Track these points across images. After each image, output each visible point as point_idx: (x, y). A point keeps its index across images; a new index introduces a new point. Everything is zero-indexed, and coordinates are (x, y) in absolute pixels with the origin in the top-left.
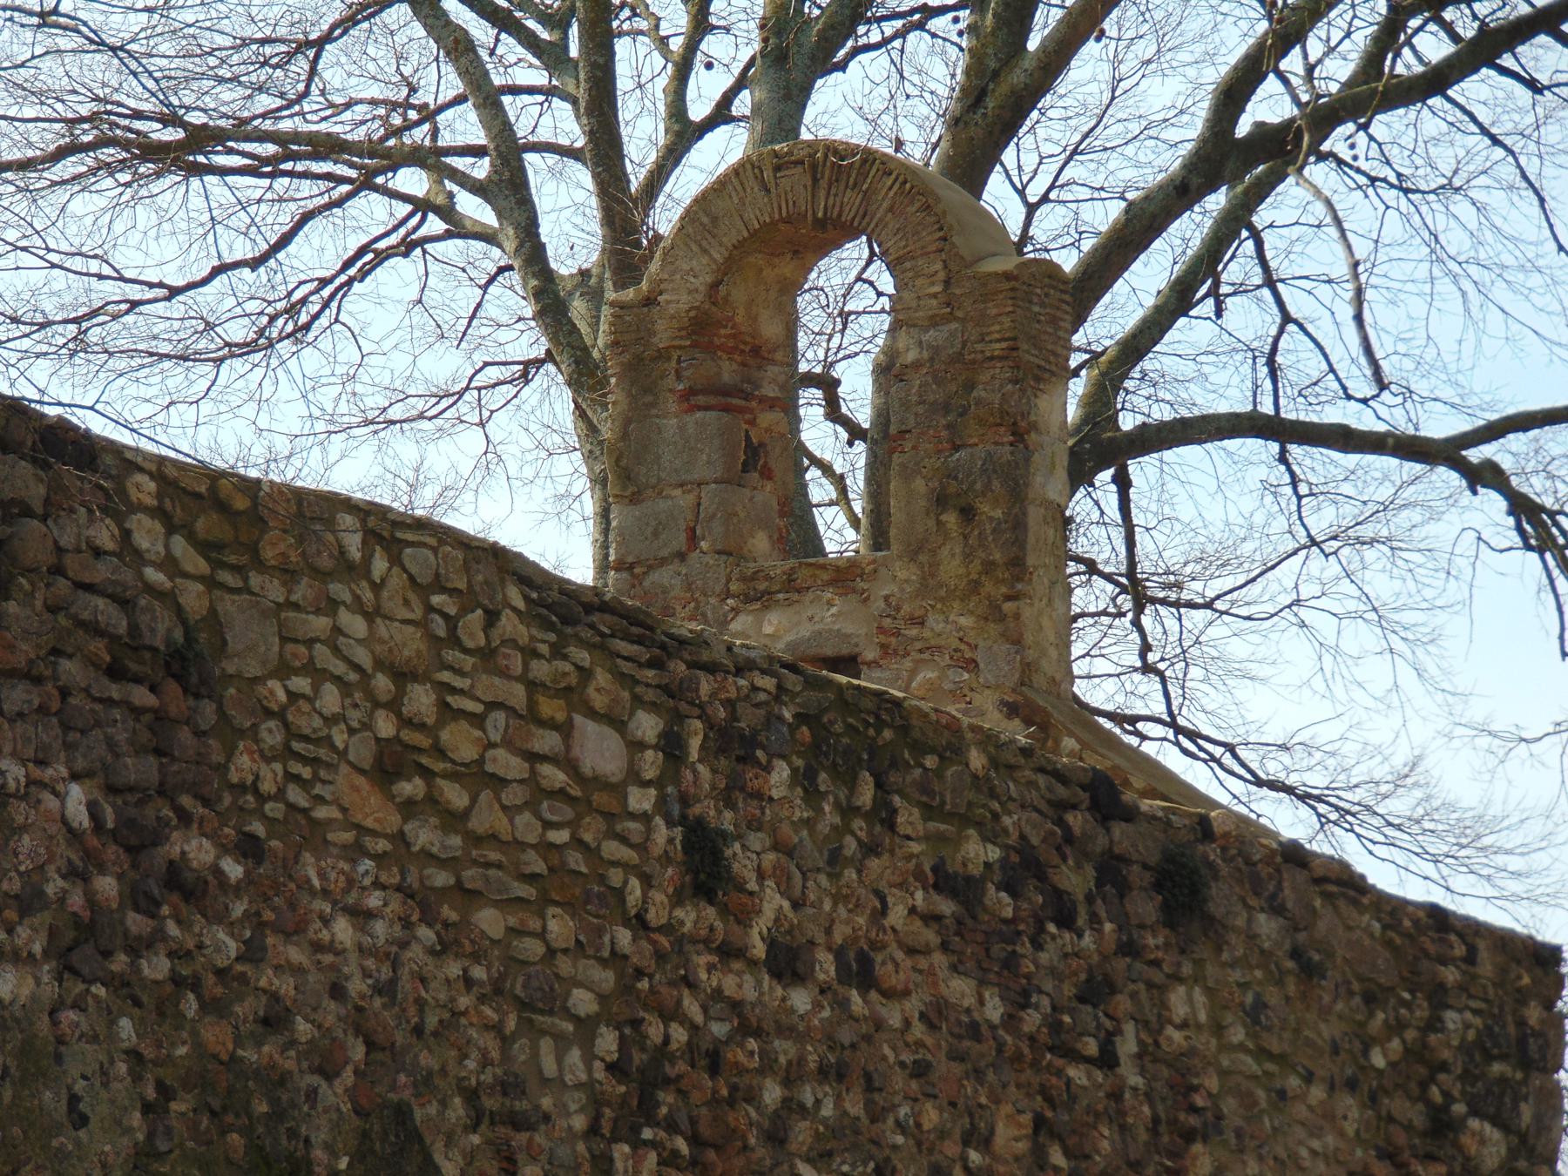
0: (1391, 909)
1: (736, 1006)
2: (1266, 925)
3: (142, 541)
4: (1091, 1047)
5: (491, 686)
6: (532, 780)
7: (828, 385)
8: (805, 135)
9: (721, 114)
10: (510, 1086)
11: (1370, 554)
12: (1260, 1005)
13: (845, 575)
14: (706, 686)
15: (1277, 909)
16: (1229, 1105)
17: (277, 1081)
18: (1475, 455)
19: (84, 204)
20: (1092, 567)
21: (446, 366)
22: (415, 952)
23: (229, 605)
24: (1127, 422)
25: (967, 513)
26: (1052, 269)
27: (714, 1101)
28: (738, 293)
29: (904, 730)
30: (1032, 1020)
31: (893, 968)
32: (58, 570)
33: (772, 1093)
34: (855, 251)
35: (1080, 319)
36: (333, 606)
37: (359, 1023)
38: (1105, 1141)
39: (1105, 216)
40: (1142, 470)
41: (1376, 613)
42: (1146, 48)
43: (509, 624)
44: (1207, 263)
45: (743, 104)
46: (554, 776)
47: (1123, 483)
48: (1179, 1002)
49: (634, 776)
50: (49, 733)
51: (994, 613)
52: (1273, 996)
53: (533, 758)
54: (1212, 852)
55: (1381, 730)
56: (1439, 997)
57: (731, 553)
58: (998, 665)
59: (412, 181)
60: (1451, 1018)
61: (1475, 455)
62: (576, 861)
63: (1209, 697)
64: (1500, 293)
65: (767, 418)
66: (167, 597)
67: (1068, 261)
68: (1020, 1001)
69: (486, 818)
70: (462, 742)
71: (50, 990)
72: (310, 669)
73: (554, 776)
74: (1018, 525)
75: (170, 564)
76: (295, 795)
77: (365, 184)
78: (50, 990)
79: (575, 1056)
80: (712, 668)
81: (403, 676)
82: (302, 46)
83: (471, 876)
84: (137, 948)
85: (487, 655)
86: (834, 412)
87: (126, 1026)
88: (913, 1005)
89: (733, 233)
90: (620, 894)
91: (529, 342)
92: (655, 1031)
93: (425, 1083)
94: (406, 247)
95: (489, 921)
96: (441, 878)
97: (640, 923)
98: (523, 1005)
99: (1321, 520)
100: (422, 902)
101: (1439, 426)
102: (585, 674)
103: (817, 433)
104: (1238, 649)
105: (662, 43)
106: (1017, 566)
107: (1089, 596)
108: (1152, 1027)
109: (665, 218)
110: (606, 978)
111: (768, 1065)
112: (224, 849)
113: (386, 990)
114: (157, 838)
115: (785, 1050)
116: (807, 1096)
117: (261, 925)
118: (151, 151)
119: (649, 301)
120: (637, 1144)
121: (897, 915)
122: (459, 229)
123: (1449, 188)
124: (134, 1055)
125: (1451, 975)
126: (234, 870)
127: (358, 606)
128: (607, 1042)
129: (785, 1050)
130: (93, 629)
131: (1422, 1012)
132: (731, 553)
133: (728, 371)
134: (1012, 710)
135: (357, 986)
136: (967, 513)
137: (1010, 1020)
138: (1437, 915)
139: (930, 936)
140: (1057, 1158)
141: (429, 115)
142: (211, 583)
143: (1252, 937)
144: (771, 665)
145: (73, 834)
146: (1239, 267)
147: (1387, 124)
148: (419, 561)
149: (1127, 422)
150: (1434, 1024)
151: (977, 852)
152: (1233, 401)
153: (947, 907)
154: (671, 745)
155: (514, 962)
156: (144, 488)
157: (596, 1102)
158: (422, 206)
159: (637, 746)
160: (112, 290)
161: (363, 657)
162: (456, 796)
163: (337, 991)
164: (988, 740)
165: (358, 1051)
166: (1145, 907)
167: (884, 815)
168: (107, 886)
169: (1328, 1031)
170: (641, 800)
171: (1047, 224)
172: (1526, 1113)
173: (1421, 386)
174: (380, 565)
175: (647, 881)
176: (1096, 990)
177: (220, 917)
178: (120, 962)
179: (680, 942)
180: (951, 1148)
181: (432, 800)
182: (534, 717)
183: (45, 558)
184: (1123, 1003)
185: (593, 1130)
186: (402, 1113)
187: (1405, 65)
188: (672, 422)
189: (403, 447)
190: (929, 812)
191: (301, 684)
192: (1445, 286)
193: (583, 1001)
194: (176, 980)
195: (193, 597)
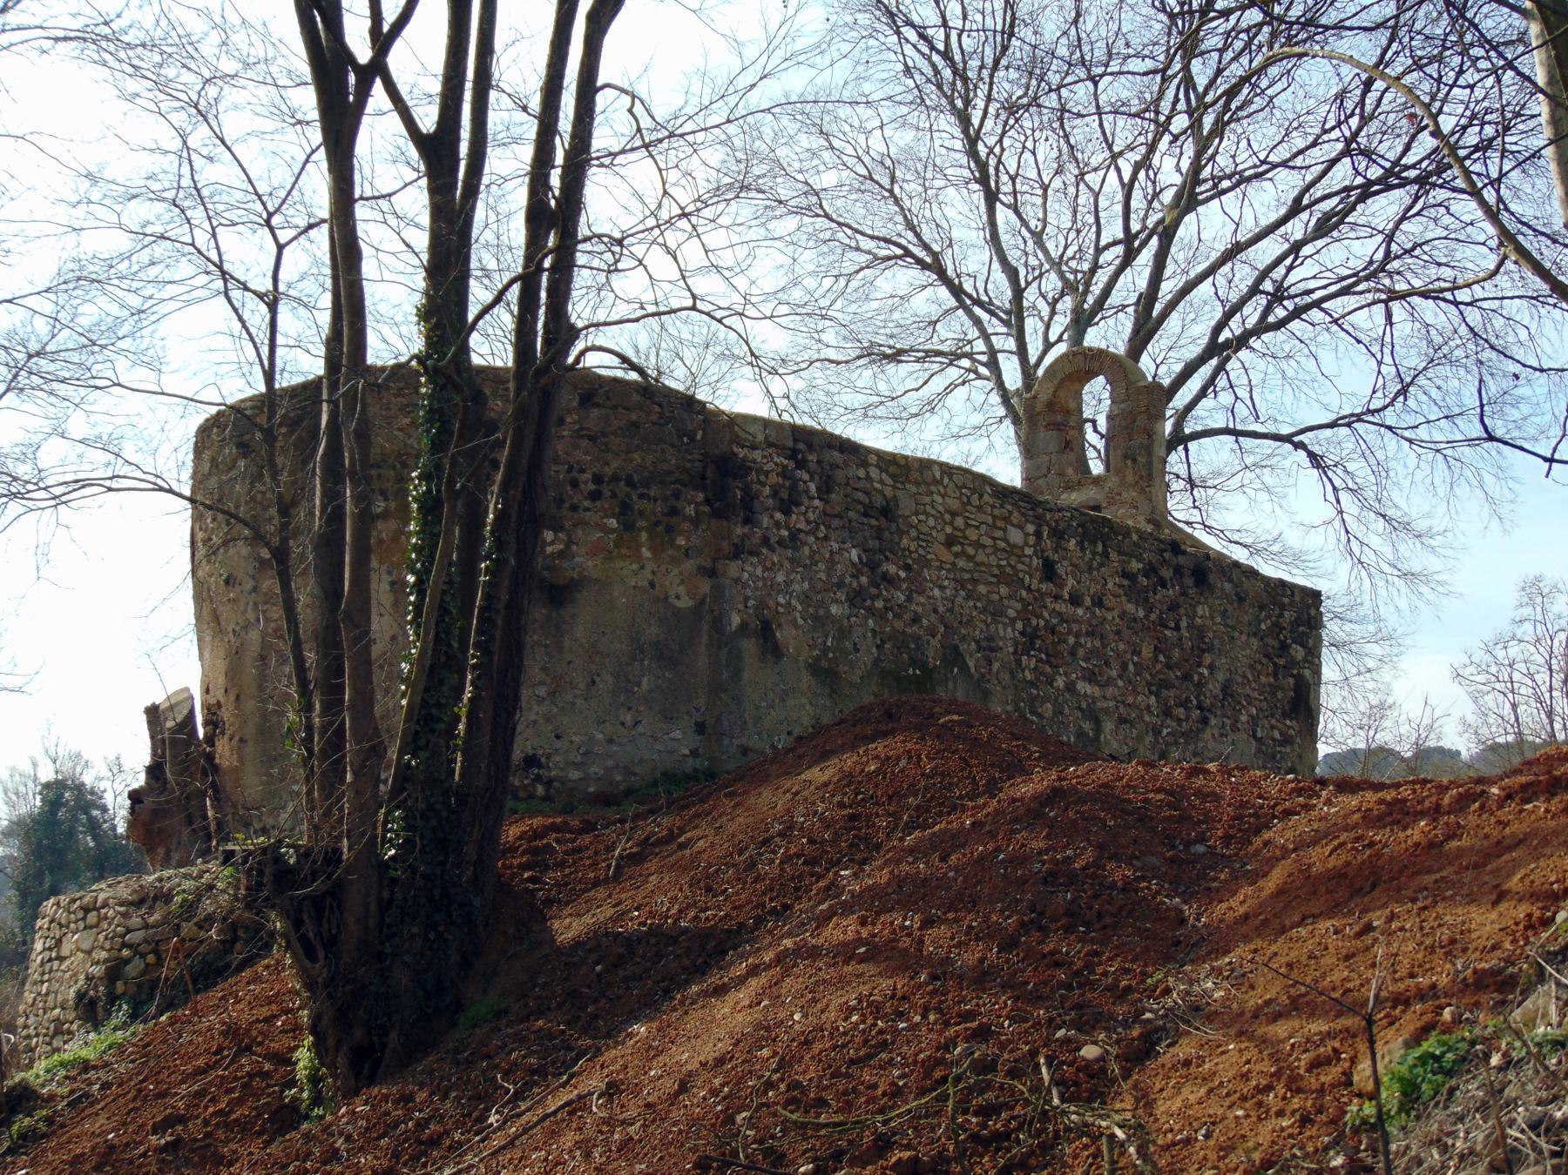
0: (1267, 580)
1: (1060, 614)
2: (1227, 586)
3: (873, 475)
4: (1172, 624)
5: (981, 517)
6: (994, 546)
7: (1094, 422)
8: (1086, 344)
9: (1060, 340)
10: (990, 639)
11: (1266, 470)
12: (1226, 610)
13: (1097, 480)
14: (1048, 516)
15: (1230, 581)
16: (1216, 642)
17: (917, 638)
18: (1296, 439)
19: (868, 373)
20: (1178, 476)
21: (977, 419)
22: (959, 599)
23: (900, 494)
24: (1187, 431)
25: (1134, 460)
26: (1160, 386)
27: (1053, 643)
28: (1062, 394)
29: (1112, 528)
30: (1153, 616)
31: (1109, 601)
32: (847, 484)
33: (1071, 640)
34: (1101, 379)
35: (1170, 400)
36: (932, 493)
37: (942, 620)
38: (1176, 653)
39: (1178, 368)
40: (1192, 445)
41: (1267, 489)
42: (1192, 316)
43: (986, 498)
44: (1211, 381)
45: (1065, 336)
46: (1002, 545)
47: (1186, 450)
48: (1200, 610)
49: (1026, 544)
50: (846, 534)
51: (1143, 491)
52: (1230, 608)
53: (995, 539)
54: (1210, 564)
55: (1269, 525)
56: (1282, 607)
57: (1061, 474)
58: (1145, 507)
59: (965, 363)
60: (1286, 614)
61: (1296, 439)
62: (1009, 570)
63: (1215, 515)
64: (1305, 389)
65: (1072, 432)
66: (881, 492)
67: (1166, 382)
68: (1149, 611)
69: (981, 557)
70: (972, 534)
71: (847, 611)
72: (925, 513)
73: (1002, 545)
74: (1150, 464)
75: (881, 482)
76: (921, 551)
77: (951, 364)
78: (847, 611)
79: (1009, 630)
80: (1050, 510)
81: (954, 514)
82: (930, 323)
83: (976, 576)
84: (874, 598)
85: (980, 508)
86: (1096, 430)
87: (871, 622)
88: (1115, 613)
89: (1060, 375)
90: (1022, 580)
91: (1002, 412)
92: (1034, 622)
93: (963, 639)
94: (964, 383)
95: (982, 589)
96: (967, 576)
97: (1029, 589)
98: (993, 614)
99: (1249, 460)
100: (961, 584)
101: (1285, 430)
102: (1010, 513)
103: (1091, 437)
104: (1224, 501)
105: (1041, 318)
106: (1150, 476)
107: (1177, 485)
108: (1191, 617)
109: (1040, 372)
110: (1019, 606)
111: (1070, 631)
112: (899, 568)
113: (951, 610)
114: (879, 565)
115: (1075, 627)
116: (1082, 641)
117: (911, 591)
118: (886, 356)
119: (1034, 397)
120: (1029, 656)
121: (1110, 585)
122: (979, 377)
123: (1288, 357)
124: (873, 631)
125: (1286, 600)
126: (903, 574)
127: (939, 493)
128: (1019, 625)
129: (1075, 627)
130: (859, 502)
131: (1277, 612)
132: (1061, 474)
133: (1059, 418)
134: (1149, 521)
135: (941, 609)
136: (1134, 460)
137: (1146, 617)
138: (1282, 582)
139: (1121, 591)
140: (1161, 658)
141: (970, 342)
142: (894, 487)
143: (1223, 590)
144: (1069, 509)
145: (854, 564)
146: (1222, 382)
147: (1266, 337)
148: (958, 479)
149: (1187, 431)
150: (1281, 615)
151: (1135, 566)
152: (1221, 424)
153: (1126, 582)
154: (1038, 534)
155: (990, 602)
156: (873, 459)
157: (1016, 644)
158: (968, 370)
159: (1027, 535)
160: (876, 399)
161: (941, 509)
162: (971, 551)
163: (935, 611)
164: (1138, 531)
165: (942, 629)
166: (1189, 581)
167: (1105, 554)
168: (864, 580)
169: (1246, 618)
170: (1029, 551)
171: (1162, 370)
172: (1311, 642)
173: (1280, 418)
174: (946, 480)
175: (1031, 576)
176: (1173, 607)
177: (899, 588)
178: (868, 602)
179: (1042, 594)
180: (1128, 656)
181: (964, 552)
182: (994, 526)
183: (844, 481)
184: (1182, 611)
185: (1015, 652)
186: (956, 648)
187: (1271, 319)
188: (1042, 434)
189: (964, 444)
190: (1120, 553)
191: (922, 517)
192: (1287, 387)
193: (1012, 613)
194: (886, 608)
195: (889, 492)
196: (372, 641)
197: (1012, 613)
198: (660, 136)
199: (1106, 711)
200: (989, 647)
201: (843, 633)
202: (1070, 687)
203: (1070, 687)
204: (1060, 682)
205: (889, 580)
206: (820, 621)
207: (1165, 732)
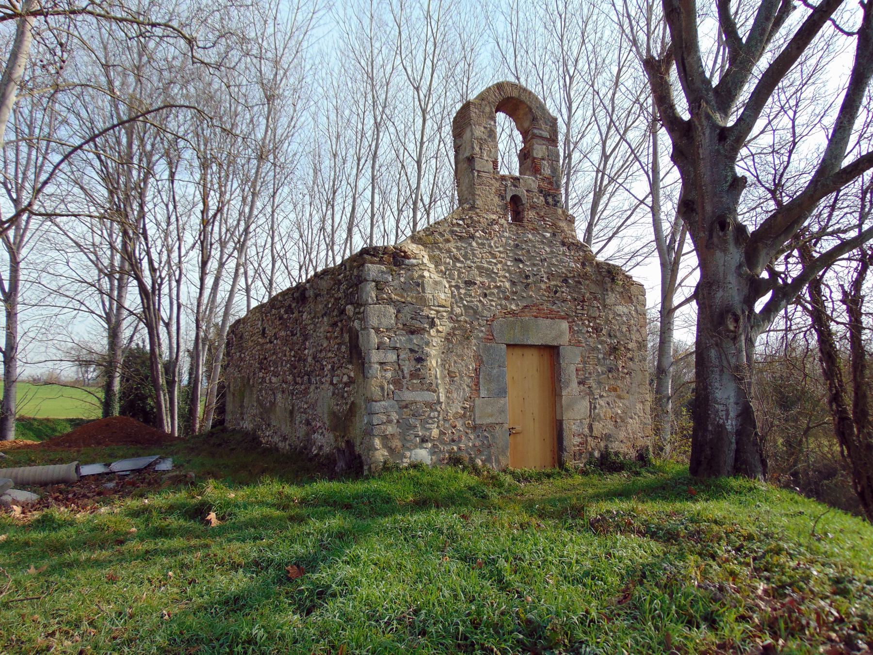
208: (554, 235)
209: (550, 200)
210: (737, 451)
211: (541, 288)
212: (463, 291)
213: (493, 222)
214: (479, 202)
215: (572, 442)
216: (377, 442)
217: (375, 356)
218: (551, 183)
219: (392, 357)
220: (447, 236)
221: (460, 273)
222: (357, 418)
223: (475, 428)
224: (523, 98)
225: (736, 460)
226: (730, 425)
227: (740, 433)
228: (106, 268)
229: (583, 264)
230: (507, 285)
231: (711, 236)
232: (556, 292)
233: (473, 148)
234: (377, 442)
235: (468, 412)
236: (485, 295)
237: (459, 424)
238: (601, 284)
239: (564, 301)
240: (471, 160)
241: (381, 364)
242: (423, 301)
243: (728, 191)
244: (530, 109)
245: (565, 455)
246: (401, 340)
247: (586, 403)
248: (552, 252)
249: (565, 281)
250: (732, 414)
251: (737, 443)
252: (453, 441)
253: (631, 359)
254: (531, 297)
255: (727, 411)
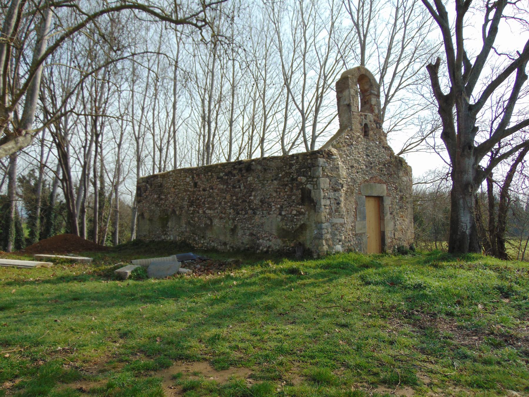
17: (166, 209)
111: (202, 198)
196: (475, 130)
197: (186, 198)
198: (249, 71)
199: (214, 216)
200: (181, 208)
201: (154, 212)
202: (204, 212)
203: (204, 212)
204: (201, 212)
205: (162, 199)
206: (151, 211)
207: (237, 219)
208: (380, 143)
209: (378, 126)
210: (470, 243)
211: (376, 169)
212: (350, 171)
213: (359, 137)
214: (353, 127)
215: (388, 241)
216: (324, 242)
217: (323, 202)
218: (378, 117)
219: (328, 202)
220: (344, 144)
221: (349, 162)
222: (308, 231)
223: (356, 235)
224: (367, 74)
225: (470, 246)
226: (468, 232)
227: (471, 235)
228: (42, 141)
229: (390, 157)
230: (364, 167)
231: (463, 151)
232: (382, 171)
233: (350, 100)
234: (324, 242)
235: (354, 228)
236: (357, 172)
237: (350, 233)
238: (397, 166)
239: (385, 175)
240: (349, 106)
241: (324, 205)
242: (339, 175)
243: (471, 132)
244: (370, 80)
245: (386, 248)
246: (332, 194)
247: (392, 223)
248: (379, 151)
249: (384, 165)
250: (468, 227)
251: (470, 239)
252: (349, 241)
253: (407, 202)
254: (373, 173)
255: (467, 226)
